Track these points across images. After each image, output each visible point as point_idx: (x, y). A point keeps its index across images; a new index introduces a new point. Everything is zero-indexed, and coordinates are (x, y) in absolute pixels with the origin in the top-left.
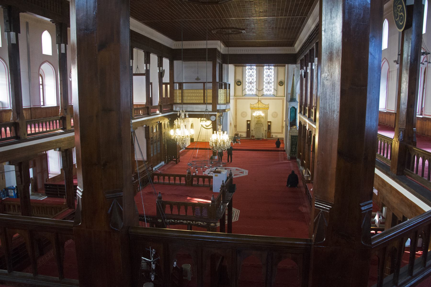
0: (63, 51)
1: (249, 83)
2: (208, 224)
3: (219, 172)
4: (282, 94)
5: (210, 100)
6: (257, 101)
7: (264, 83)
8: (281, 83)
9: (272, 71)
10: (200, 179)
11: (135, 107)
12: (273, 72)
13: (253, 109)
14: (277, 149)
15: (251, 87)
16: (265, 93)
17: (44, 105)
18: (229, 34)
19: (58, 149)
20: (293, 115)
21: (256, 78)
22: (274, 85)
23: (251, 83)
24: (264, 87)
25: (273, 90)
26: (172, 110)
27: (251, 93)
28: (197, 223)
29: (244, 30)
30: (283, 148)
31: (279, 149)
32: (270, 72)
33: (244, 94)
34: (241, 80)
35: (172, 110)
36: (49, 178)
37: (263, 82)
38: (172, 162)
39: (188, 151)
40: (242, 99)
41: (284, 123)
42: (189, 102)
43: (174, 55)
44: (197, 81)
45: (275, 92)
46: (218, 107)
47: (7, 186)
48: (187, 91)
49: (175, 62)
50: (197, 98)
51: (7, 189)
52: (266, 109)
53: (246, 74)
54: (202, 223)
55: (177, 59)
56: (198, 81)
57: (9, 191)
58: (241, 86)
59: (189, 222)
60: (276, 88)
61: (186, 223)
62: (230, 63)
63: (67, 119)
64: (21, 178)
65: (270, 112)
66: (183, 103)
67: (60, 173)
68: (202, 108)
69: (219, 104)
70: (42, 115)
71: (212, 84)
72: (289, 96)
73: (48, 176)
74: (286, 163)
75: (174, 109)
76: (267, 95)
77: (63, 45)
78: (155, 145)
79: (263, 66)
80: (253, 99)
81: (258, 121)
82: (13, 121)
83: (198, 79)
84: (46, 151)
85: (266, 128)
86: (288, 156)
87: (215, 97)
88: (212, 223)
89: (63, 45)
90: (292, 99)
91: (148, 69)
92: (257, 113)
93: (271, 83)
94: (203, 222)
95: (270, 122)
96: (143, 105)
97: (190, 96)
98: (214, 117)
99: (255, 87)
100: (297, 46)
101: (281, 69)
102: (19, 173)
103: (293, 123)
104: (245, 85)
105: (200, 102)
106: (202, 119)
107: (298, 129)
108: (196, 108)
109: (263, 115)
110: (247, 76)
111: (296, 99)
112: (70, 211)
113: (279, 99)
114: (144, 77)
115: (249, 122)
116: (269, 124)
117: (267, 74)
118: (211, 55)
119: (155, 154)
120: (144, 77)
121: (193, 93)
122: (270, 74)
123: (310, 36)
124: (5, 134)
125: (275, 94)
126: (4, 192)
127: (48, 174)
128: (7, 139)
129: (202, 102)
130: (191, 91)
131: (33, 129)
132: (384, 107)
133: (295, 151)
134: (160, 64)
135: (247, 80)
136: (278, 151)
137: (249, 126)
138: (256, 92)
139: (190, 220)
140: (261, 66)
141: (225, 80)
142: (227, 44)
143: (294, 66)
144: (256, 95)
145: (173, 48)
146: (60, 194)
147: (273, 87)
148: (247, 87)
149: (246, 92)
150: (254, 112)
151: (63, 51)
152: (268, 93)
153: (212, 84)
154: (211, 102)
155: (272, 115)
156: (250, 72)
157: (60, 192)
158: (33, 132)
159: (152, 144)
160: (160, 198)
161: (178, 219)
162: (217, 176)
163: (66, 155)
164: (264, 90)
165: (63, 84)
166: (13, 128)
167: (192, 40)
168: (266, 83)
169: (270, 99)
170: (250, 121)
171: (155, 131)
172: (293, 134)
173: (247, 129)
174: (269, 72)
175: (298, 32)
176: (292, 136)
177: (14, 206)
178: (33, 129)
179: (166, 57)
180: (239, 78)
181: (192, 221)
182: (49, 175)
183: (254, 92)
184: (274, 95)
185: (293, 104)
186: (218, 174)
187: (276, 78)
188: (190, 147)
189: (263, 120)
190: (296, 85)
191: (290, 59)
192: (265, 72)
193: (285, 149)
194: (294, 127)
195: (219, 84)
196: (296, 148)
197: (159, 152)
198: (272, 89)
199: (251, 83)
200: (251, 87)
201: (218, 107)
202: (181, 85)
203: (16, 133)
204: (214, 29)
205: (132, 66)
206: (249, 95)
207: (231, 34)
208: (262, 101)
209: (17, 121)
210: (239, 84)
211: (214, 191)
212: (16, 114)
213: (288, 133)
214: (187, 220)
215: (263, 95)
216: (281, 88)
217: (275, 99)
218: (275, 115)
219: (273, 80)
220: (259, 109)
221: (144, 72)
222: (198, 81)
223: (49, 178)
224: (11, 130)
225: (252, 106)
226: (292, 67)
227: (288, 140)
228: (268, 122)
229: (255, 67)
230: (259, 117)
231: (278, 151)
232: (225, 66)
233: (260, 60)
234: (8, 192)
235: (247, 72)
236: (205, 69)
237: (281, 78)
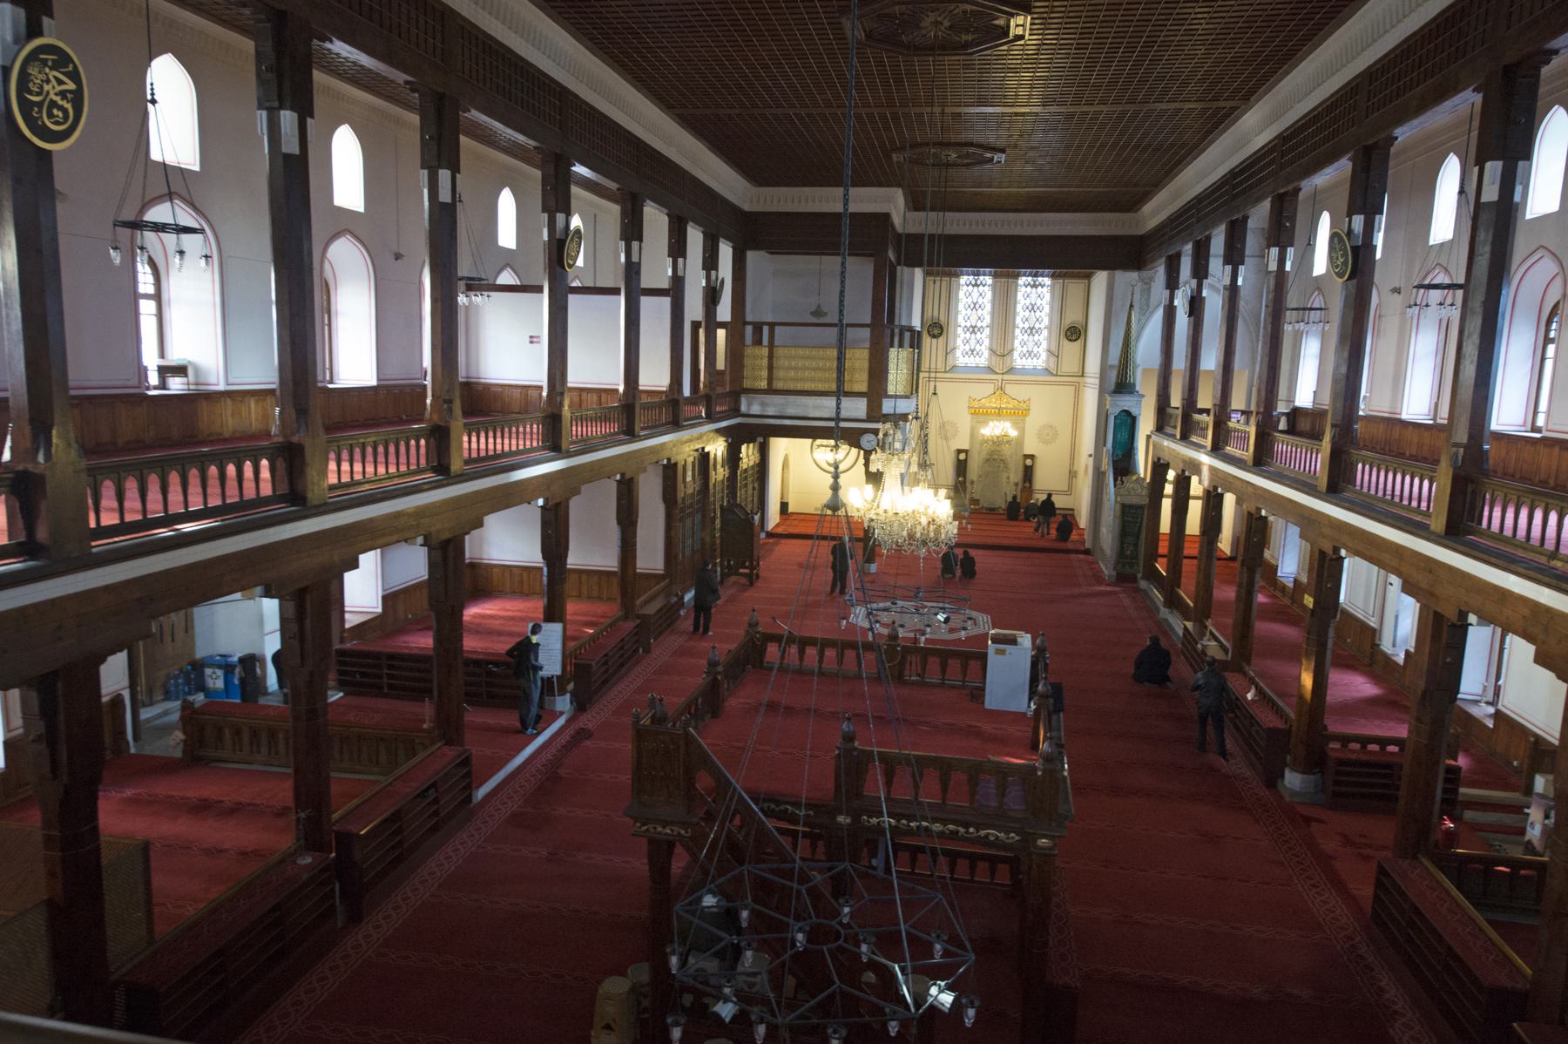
0: (445, 196)
1: (966, 329)
2: (1028, 838)
3: (1013, 641)
5: (860, 382)
6: (990, 388)
9: (1045, 292)
10: (931, 659)
11: (645, 399)
12: (1048, 296)
13: (980, 414)
14: (1062, 545)
15: (973, 342)
17: (331, 382)
18: (948, 165)
19: (420, 540)
20: (1124, 435)
21: (993, 314)
22: (1049, 339)
23: (973, 329)
24: (1017, 343)
25: (1044, 356)
26: (735, 412)
27: (972, 361)
28: (983, 833)
29: (1003, 151)
30: (1083, 542)
31: (1070, 546)
32: (1036, 296)
33: (950, 363)
35: (735, 412)
36: (347, 626)
37: (1015, 326)
38: (733, 579)
39: (776, 544)
40: (951, 380)
42: (791, 386)
43: (753, 233)
44: (815, 320)
45: (1053, 360)
46: (887, 407)
47: (201, 653)
48: (786, 351)
49: (752, 256)
50: (819, 374)
51: (199, 666)
53: (957, 301)
54: (1002, 835)
55: (757, 247)
56: (822, 321)
57: (208, 671)
59: (951, 827)
60: (1054, 349)
61: (942, 832)
63: (453, 435)
64: (302, 641)
65: (1033, 422)
66: (771, 391)
67: (380, 610)
68: (826, 406)
69: (891, 397)
70: (484, 404)
71: (868, 330)
72: (1113, 376)
73: (343, 620)
74: (1110, 593)
75: (743, 409)
76: (1024, 371)
77: (444, 175)
78: (688, 522)
79: (1017, 276)
80: (979, 381)
81: (992, 453)
82: (280, 439)
83: (818, 313)
84: (846, 618)
85: (1015, 475)
86: (1107, 571)
87: (878, 372)
88: (1045, 836)
90: (1123, 386)
91: (680, 273)
92: (994, 429)
93: (1038, 331)
94: (1007, 833)
95: (1032, 457)
96: (661, 392)
97: (795, 369)
98: (871, 437)
99: (987, 342)
100: (1156, 211)
101: (1075, 287)
102: (294, 627)
103: (1123, 464)
104: (956, 336)
105: (820, 387)
106: (819, 442)
108: (816, 407)
109: (1013, 433)
110: (961, 306)
111: (1134, 385)
112: (451, 752)
114: (666, 302)
115: (962, 457)
116: (1029, 462)
117: (1028, 302)
118: (870, 236)
119: (688, 552)
120: (666, 302)
121: (805, 362)
122: (1039, 302)
124: (253, 485)
126: (187, 675)
127: (343, 612)
128: (260, 502)
129: (834, 387)
130: (793, 351)
131: (358, 467)
132: (1521, 421)
133: (1135, 557)
134: (710, 263)
135: (960, 319)
136: (1068, 551)
138: (1048, 361)
139: (954, 822)
140: (1008, 276)
142: (916, 203)
143: (1134, 275)
144: (990, 370)
145: (746, 207)
146: (391, 686)
147: (1044, 345)
148: (959, 342)
149: (955, 359)
150: (985, 423)
151: (445, 196)
152: (1028, 363)
153: (868, 330)
154: (863, 387)
155: (1039, 436)
156: (973, 295)
157: (380, 677)
158: (345, 479)
159: (681, 520)
160: (849, 738)
161: (910, 818)
162: (1002, 652)
163: (445, 559)
166: (281, 464)
167: (821, 186)
168: (1024, 331)
169: (1036, 383)
170: (966, 451)
171: (689, 479)
174: (1034, 296)
175: (1179, 162)
177: (237, 732)
178: (358, 467)
179: (728, 238)
181: (966, 825)
182: (347, 616)
183: (983, 361)
184: (1047, 371)
185: (1126, 402)
186: (1009, 648)
188: (780, 530)
189: (1007, 450)
191: (1129, 254)
192: (1020, 296)
193: (1088, 545)
195: (886, 328)
196: (1136, 545)
197: (697, 546)
198: (1042, 351)
199: (973, 329)
200: (973, 342)
201: (887, 407)
202: (758, 327)
203: (291, 483)
204: (902, 148)
205: (639, 264)
206: (967, 369)
208: (1009, 389)
209: (295, 439)
210: (936, 332)
211: (988, 705)
212: (293, 412)
214: (944, 822)
215: (1011, 370)
218: (1049, 434)
219: (1046, 321)
220: (999, 414)
221: (665, 285)
222: (818, 319)
223: (347, 626)
224: (273, 470)
225: (976, 404)
228: (1027, 457)
229: (989, 280)
230: (999, 442)
231: (1068, 551)
233: (1007, 258)
234: (202, 674)
235: (961, 294)
236: (849, 281)
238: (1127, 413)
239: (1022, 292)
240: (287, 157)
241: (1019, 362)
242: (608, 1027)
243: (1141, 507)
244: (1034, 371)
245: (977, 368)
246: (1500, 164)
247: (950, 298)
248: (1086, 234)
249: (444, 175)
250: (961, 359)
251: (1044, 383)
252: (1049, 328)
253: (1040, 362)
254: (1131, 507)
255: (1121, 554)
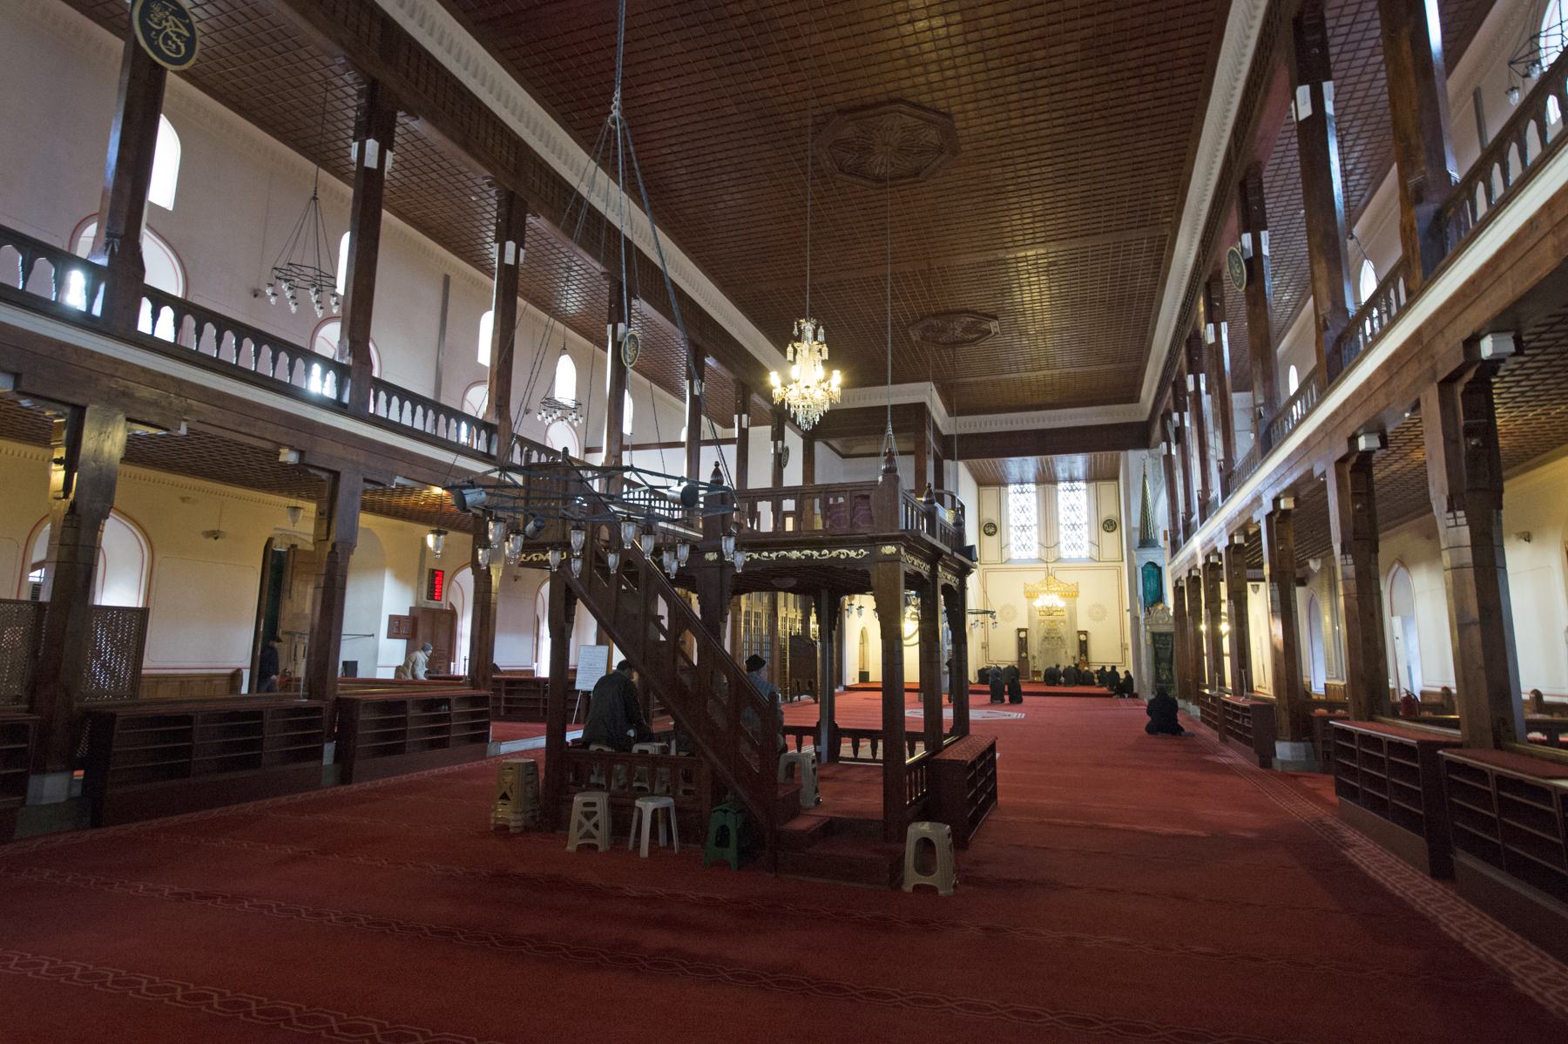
4: (1115, 554)
6: (1042, 575)
7: (1061, 528)
8: (1110, 525)
16: (1065, 554)
20: (1153, 585)
24: (1062, 538)
28: (834, 554)
34: (995, 521)
40: (1000, 570)
41: (1128, 616)
45: (1095, 549)
52: (1071, 594)
54: (853, 554)
58: (995, 538)
59: (808, 552)
60: (1094, 539)
62: (961, 458)
72: (1137, 537)
80: (1032, 569)
81: (1049, 631)
89: (510, 246)
95: (1085, 633)
107: (1171, 612)
110: (1011, 510)
113: (1107, 568)
115: (1023, 635)
116: (1083, 637)
123: (1183, 305)
125: (1095, 555)
137: (1022, 644)
141: (948, 486)
143: (1146, 452)
144: (1040, 560)
152: (1074, 554)
164: (1062, 547)
165: (502, 330)
169: (1082, 569)
172: (1157, 629)
173: (1020, 653)
176: (1154, 635)
180: (990, 515)
185: (1150, 555)
187: (1094, 513)
189: (1062, 629)
190: (1155, 506)
194: (1160, 607)
196: (1170, 670)
206: (1020, 561)
207: (963, 342)
208: (1059, 575)
213: (1142, 628)
215: (1059, 560)
216: (1110, 539)
217: (1095, 569)
218: (1098, 613)
226: (1134, 460)
227: (1144, 667)
228: (1080, 633)
230: (1049, 612)
232: (948, 464)
237: (1109, 511)
238: (1153, 564)
239: (1062, 496)
240: (368, 169)
241: (1065, 553)
242: (505, 797)
243: (1171, 634)
244: (1080, 560)
245: (1030, 560)
246: (1307, 88)
247: (1000, 504)
248: (1104, 427)
249: (510, 246)
250: (1015, 553)
251: (1089, 568)
252: (1089, 523)
253: (1084, 552)
254: (1161, 634)
255: (1157, 678)
